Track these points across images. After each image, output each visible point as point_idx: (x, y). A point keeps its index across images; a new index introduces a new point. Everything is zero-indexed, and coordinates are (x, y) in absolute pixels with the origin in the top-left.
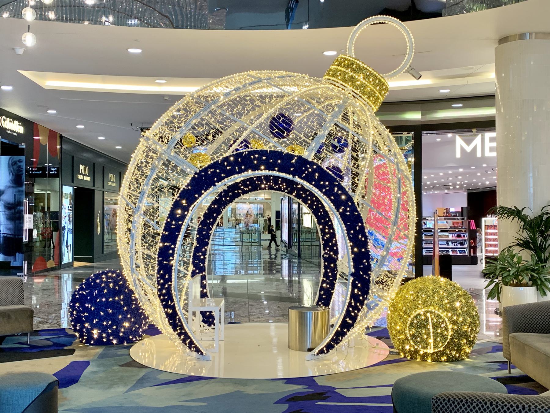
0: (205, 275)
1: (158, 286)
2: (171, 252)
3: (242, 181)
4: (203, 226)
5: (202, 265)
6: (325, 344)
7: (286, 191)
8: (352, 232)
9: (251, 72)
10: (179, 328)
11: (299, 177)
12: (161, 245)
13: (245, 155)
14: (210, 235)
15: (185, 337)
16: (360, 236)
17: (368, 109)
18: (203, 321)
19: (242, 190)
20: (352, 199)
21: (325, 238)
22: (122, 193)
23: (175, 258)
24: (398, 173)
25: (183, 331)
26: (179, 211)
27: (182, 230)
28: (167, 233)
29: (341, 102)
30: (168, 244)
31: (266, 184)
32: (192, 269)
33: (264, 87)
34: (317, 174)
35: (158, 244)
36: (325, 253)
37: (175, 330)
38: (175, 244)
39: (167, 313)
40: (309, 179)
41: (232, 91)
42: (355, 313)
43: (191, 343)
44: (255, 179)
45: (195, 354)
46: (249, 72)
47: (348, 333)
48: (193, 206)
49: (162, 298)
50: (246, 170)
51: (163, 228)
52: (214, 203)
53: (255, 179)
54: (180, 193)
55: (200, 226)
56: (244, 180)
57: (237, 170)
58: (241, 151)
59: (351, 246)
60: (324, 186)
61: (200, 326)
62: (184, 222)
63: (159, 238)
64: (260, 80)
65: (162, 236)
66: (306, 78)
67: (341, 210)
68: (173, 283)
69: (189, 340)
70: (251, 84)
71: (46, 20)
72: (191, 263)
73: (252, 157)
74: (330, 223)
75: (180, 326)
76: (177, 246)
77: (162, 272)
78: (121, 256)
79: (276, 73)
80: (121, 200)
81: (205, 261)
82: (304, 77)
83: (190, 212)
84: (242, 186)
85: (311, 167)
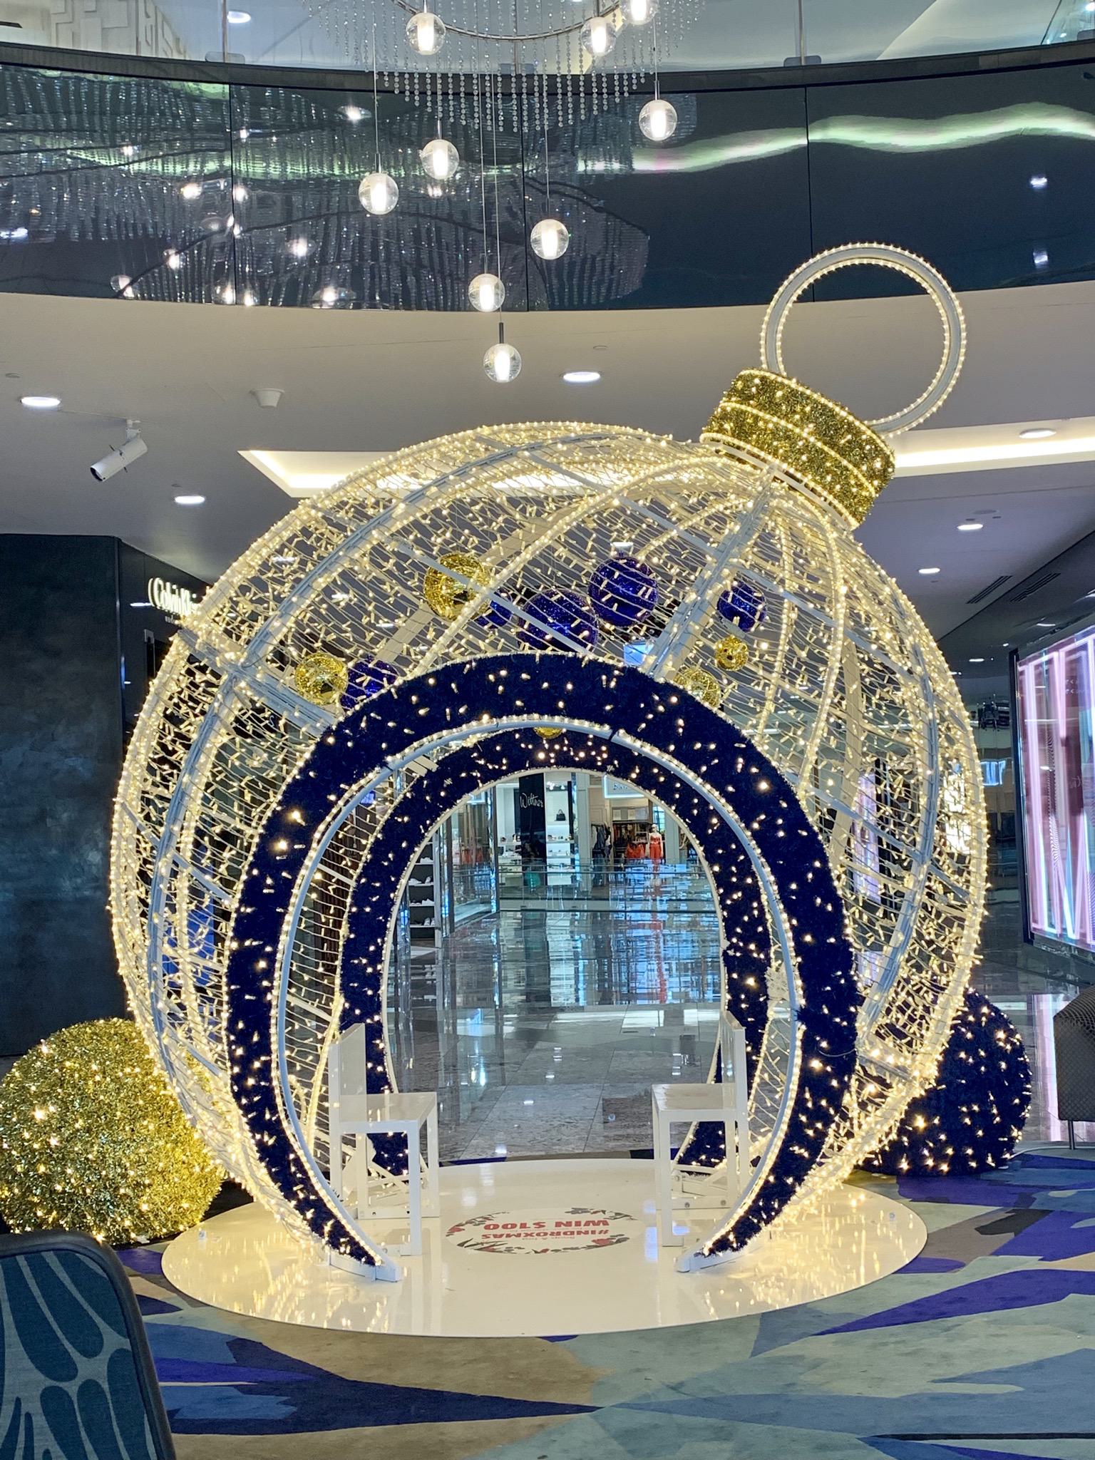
0: (379, 1024)
1: (232, 1068)
2: (262, 964)
3: (480, 742)
4: (371, 879)
5: (370, 993)
6: (732, 1223)
7: (610, 768)
8: (794, 886)
9: (485, 431)
10: (300, 1186)
11: (629, 732)
12: (235, 945)
13: (470, 670)
14: (393, 904)
15: (319, 1216)
16: (819, 901)
17: (833, 524)
18: (378, 1160)
19: (480, 768)
20: (788, 787)
21: (729, 902)
22: (124, 797)
23: (276, 983)
24: (927, 706)
25: (312, 1197)
26: (282, 845)
27: (293, 900)
28: (249, 910)
29: (750, 505)
30: (255, 943)
31: (551, 749)
32: (341, 1008)
33: (523, 472)
34: (681, 722)
35: (227, 943)
36: (732, 946)
37: (289, 1195)
38: (274, 941)
39: (261, 1146)
40: (658, 736)
41: (429, 486)
42: (816, 1130)
43: (339, 1231)
44: (517, 736)
45: (350, 1263)
46: (479, 429)
47: (798, 1189)
48: (322, 827)
49: (244, 1101)
50: (473, 715)
51: (239, 896)
52: (401, 809)
53: (517, 736)
54: (285, 792)
55: (363, 881)
56: (486, 740)
57: (448, 718)
58: (458, 661)
59: (792, 927)
60: (704, 756)
61: (369, 1174)
62: (299, 877)
63: (227, 928)
64: (509, 454)
65: (236, 920)
66: (648, 441)
67: (756, 826)
68: (274, 1056)
69: (330, 1223)
70: (483, 464)
71: (217, 303)
72: (337, 988)
73: (491, 677)
74: (742, 857)
75: (302, 1181)
76: (280, 947)
77: (241, 1025)
78: (125, 980)
79: (559, 429)
80: (121, 817)
81: (378, 981)
82: (640, 438)
83: (314, 845)
84: (479, 758)
85: (664, 701)
